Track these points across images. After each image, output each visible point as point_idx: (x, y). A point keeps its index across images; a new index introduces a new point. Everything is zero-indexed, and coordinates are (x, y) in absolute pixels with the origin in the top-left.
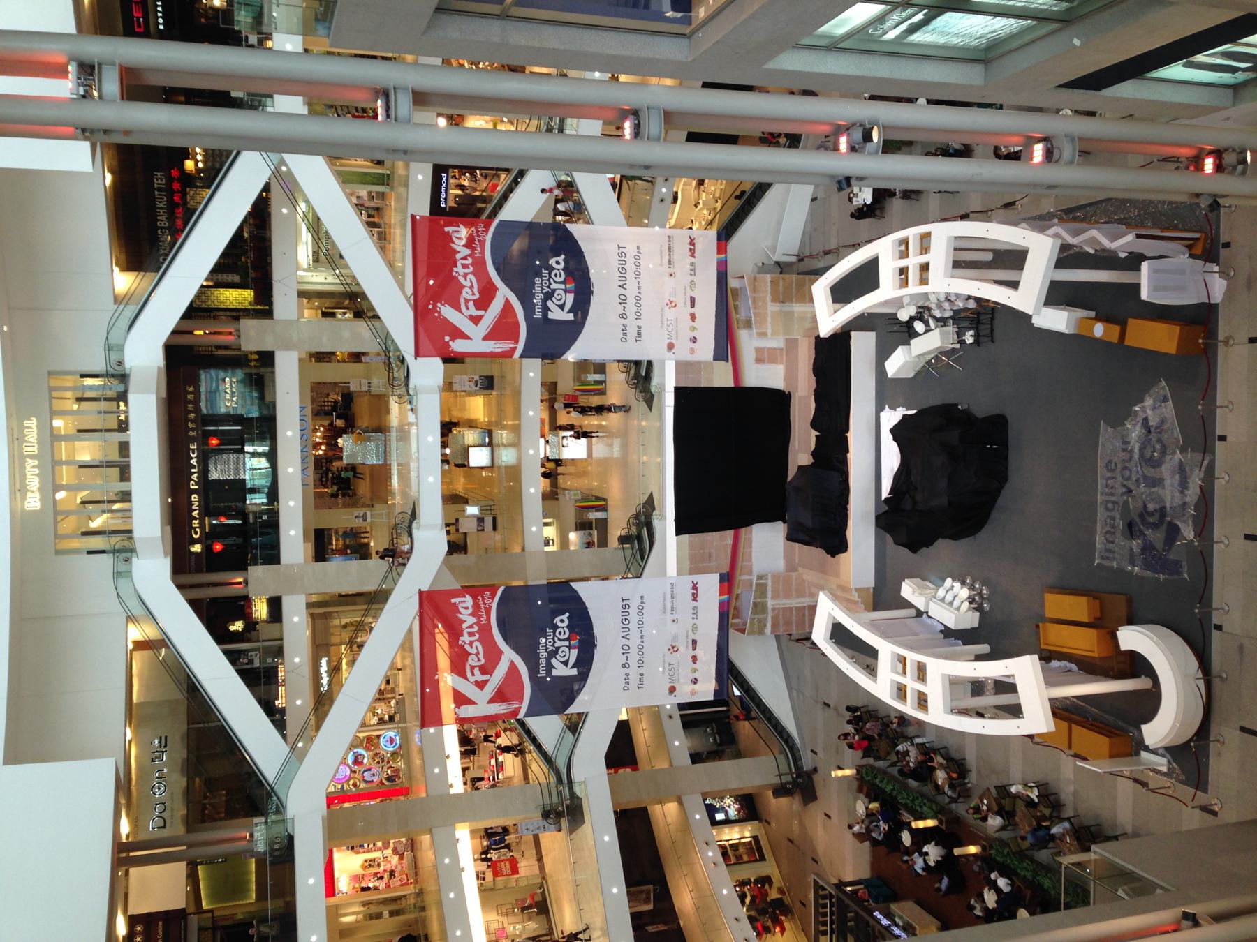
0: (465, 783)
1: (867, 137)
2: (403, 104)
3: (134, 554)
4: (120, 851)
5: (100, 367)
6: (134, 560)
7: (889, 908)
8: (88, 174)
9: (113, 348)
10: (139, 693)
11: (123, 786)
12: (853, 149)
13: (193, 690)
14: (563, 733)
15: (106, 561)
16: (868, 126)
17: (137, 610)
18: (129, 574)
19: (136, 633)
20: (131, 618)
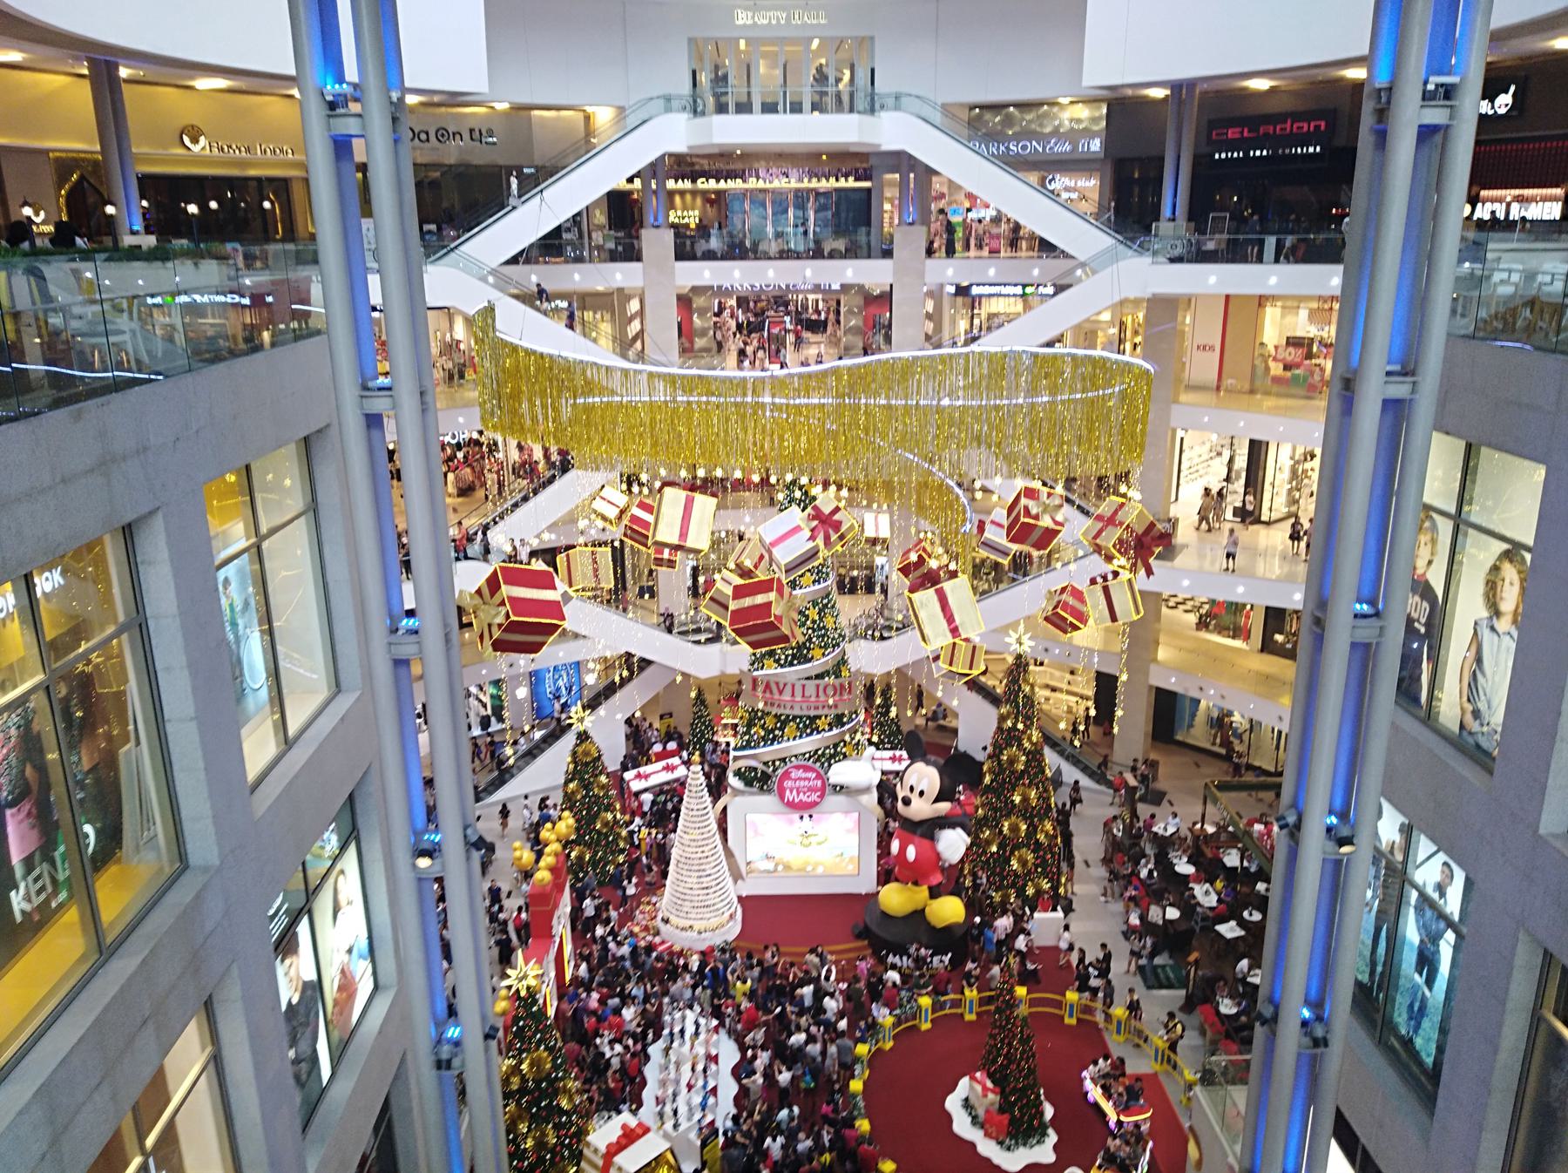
1: (1342, 842)
8: (1081, 81)
9: (898, 101)
10: (542, 118)
11: (455, 99)
12: (1329, 829)
13: (539, 176)
17: (632, 121)
18: (668, 110)
19: (603, 116)
20: (621, 110)
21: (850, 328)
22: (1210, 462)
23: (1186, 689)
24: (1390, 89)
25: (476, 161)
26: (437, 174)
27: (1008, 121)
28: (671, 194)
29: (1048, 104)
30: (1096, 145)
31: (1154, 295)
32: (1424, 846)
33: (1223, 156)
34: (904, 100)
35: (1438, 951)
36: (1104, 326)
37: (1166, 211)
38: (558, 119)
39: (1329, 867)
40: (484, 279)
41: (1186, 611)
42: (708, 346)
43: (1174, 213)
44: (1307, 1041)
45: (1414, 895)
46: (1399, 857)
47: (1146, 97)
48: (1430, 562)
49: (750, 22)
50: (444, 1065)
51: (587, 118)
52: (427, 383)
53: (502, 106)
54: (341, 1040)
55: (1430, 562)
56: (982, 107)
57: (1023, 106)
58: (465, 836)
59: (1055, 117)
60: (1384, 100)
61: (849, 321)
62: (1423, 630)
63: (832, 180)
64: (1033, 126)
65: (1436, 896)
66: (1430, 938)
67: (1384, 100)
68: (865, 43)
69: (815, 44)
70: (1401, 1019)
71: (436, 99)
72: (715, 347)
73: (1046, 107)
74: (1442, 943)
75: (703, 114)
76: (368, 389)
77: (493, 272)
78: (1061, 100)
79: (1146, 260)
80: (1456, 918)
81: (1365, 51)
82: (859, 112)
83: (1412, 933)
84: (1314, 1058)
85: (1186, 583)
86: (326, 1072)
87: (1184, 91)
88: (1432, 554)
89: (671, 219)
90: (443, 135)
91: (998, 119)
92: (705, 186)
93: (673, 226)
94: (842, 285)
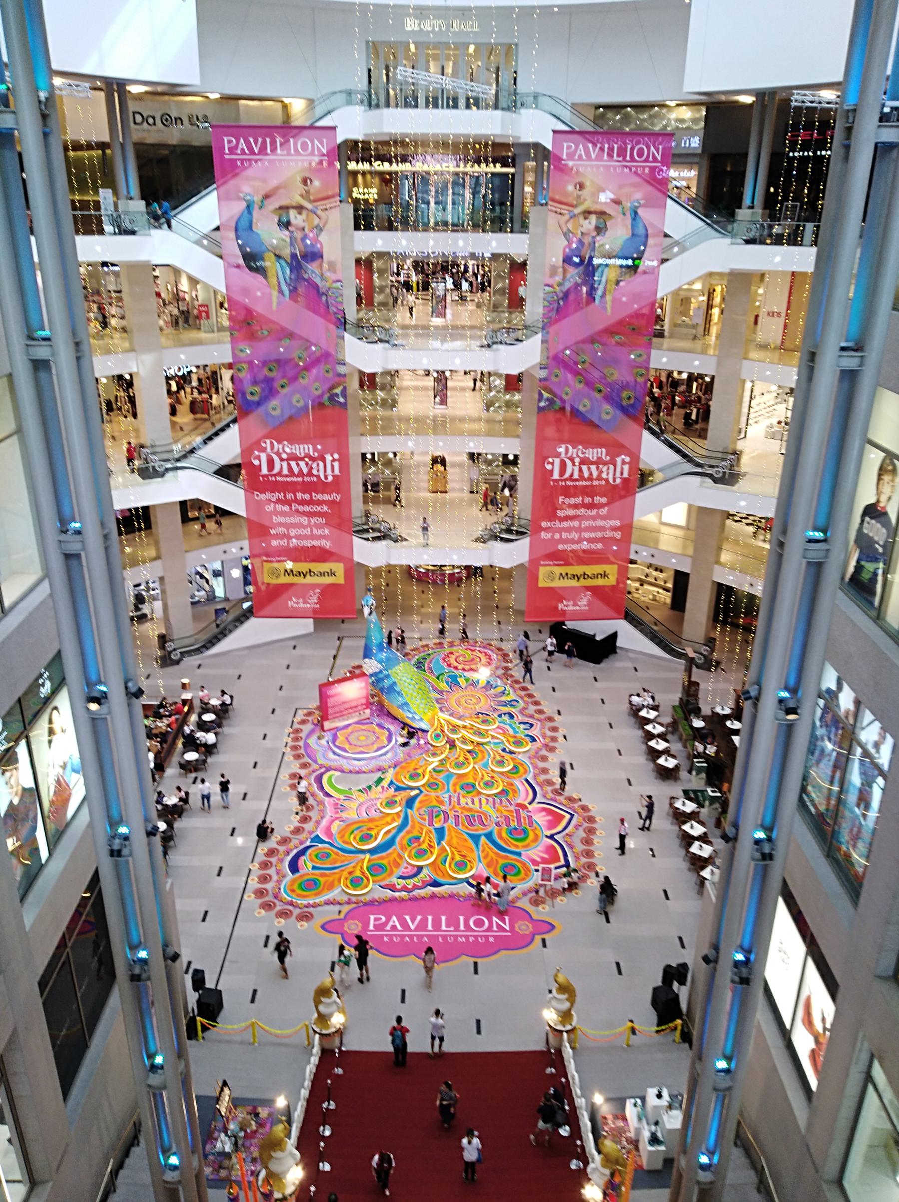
0: (548, 358)
2: (850, 362)
3: (367, 108)
4: (118, 84)
5: (521, 87)
6: (362, 108)
7: (694, 745)
10: (247, 106)
11: (173, 90)
12: (781, 701)
14: (215, 463)
15: (361, 84)
16: (799, 711)
18: (349, 103)
20: (311, 102)
21: (499, 289)
22: (775, 407)
23: (740, 585)
24: (854, 111)
25: (196, 143)
26: (166, 152)
27: (626, 119)
28: (354, 174)
29: (659, 106)
30: (695, 143)
31: (732, 270)
32: (868, 716)
33: (806, 154)
34: (541, 99)
35: (871, 792)
36: (695, 294)
37: (747, 201)
38: (262, 108)
39: (784, 728)
40: (198, 243)
41: (748, 524)
42: (384, 301)
43: (753, 202)
44: (758, 855)
45: (859, 751)
46: (851, 721)
47: (737, 102)
48: (889, 498)
49: (417, 29)
50: (116, 853)
51: (285, 107)
52: (82, 335)
53: (214, 96)
54: (57, 830)
55: (889, 498)
56: (604, 107)
57: (640, 107)
58: (127, 688)
59: (663, 117)
60: (850, 120)
61: (496, 284)
62: (880, 550)
63: (483, 165)
64: (646, 124)
65: (872, 751)
66: (867, 783)
67: (850, 120)
68: (510, 50)
69: (472, 49)
70: (844, 836)
71: (160, 89)
72: (391, 301)
73: (656, 109)
74: (875, 786)
75: (377, 106)
76: (34, 339)
77: (206, 237)
78: (668, 103)
79: (728, 241)
80: (886, 767)
81: (839, 78)
82: (503, 109)
83: (855, 778)
84: (766, 867)
85: (743, 503)
86: (44, 853)
87: (766, 98)
88: (892, 492)
89: (354, 195)
90: (167, 120)
91: (618, 117)
92: (381, 168)
93: (356, 202)
94: (492, 254)
